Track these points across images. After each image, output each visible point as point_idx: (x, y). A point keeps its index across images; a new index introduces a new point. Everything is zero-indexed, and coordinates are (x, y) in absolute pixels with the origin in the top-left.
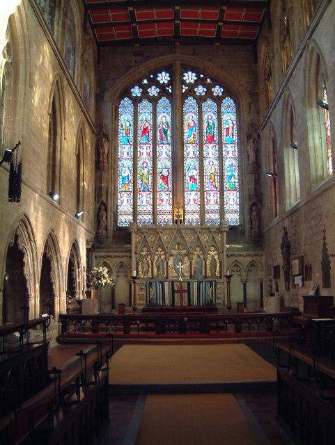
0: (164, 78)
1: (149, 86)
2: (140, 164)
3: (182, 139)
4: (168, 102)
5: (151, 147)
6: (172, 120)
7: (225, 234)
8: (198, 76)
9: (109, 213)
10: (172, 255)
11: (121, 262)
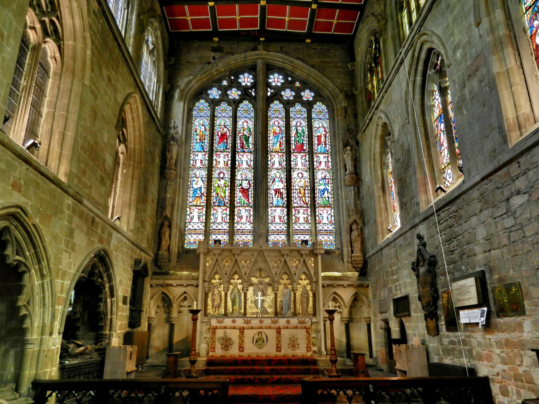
0: (246, 80)
1: (230, 87)
2: (215, 175)
3: (266, 147)
4: (250, 106)
5: (230, 155)
6: (255, 125)
7: (320, 257)
8: (285, 78)
9: (174, 230)
10: (251, 284)
11: (185, 293)
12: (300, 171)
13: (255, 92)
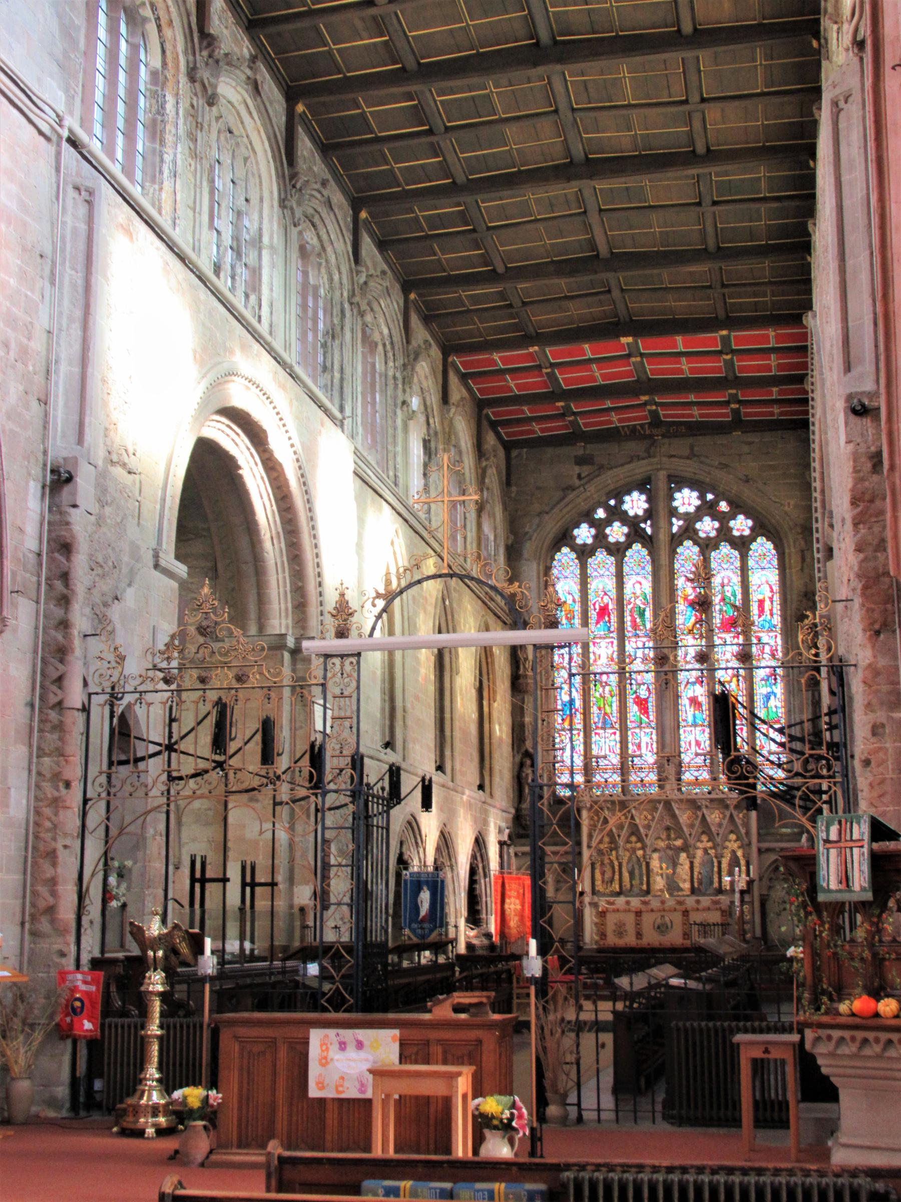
1: (608, 522)
8: (702, 497)
13: (652, 526)
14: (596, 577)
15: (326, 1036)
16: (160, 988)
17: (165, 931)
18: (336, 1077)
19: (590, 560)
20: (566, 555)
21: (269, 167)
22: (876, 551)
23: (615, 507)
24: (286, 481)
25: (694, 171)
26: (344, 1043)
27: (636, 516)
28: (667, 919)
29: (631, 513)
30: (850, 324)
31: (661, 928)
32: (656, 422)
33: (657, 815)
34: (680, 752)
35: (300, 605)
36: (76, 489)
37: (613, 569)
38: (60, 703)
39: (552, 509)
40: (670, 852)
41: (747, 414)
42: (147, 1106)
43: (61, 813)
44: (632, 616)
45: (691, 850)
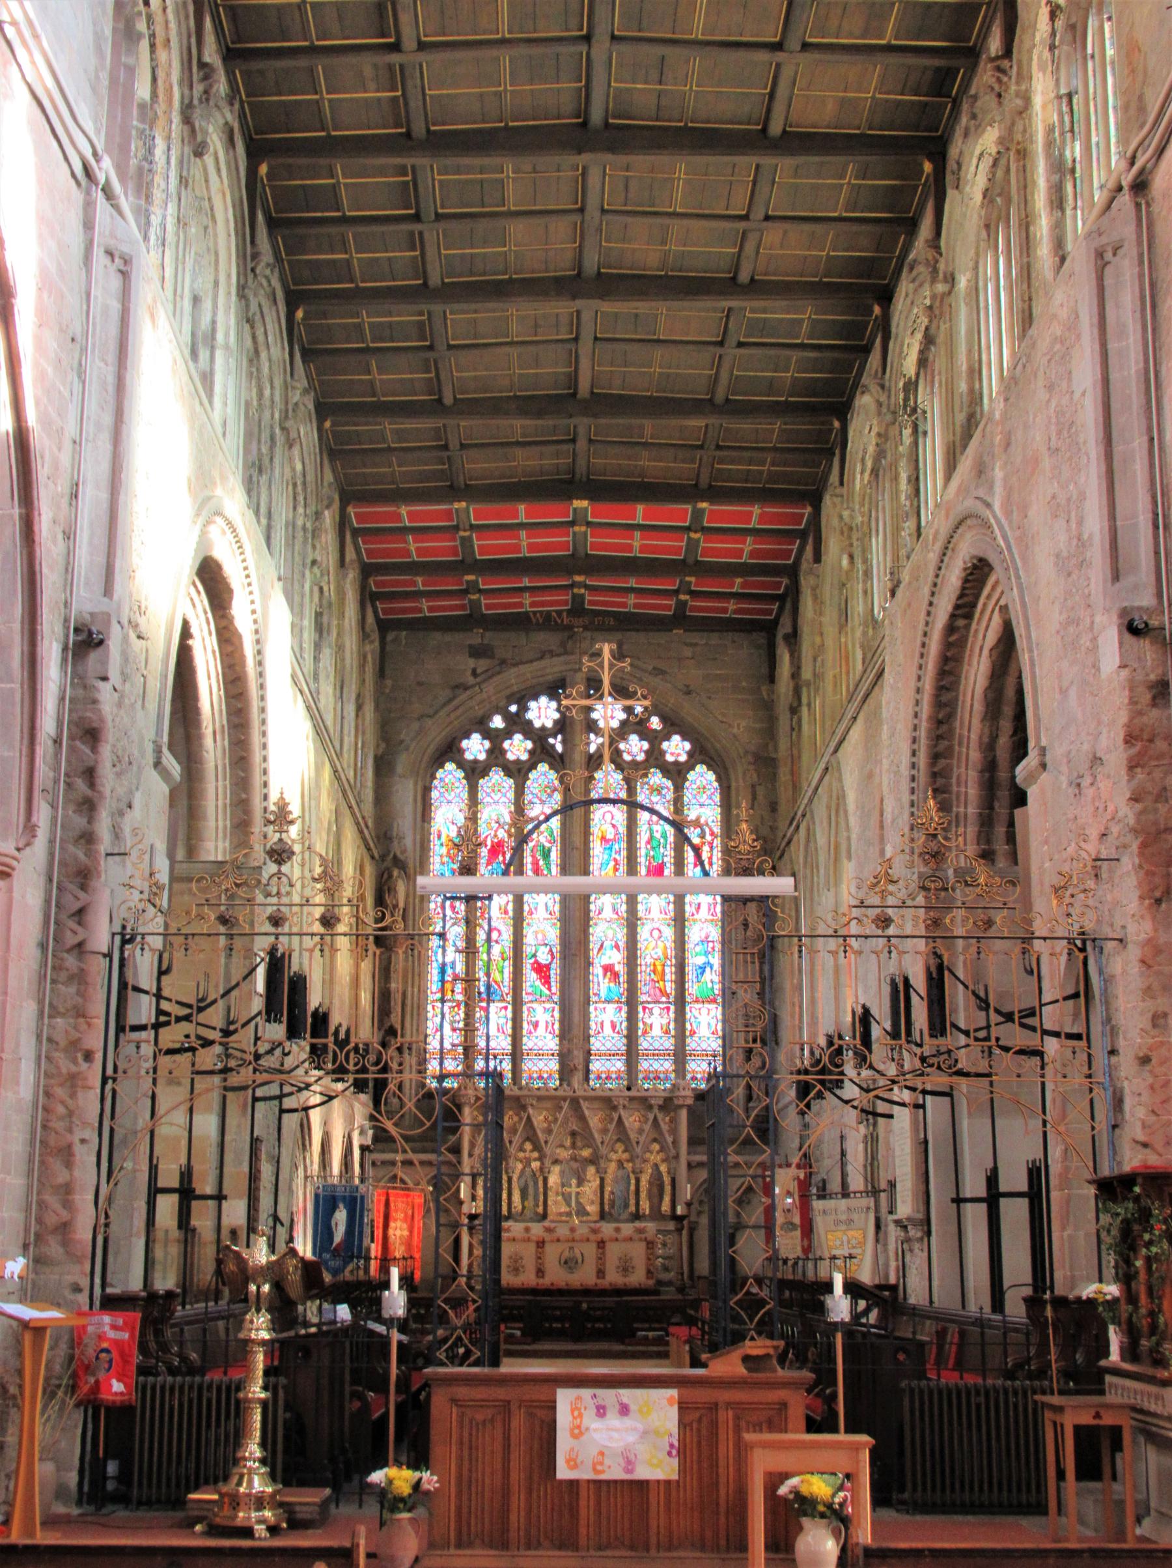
0: (543, 712)
1: (508, 734)
12: (656, 925)
13: (564, 742)
14: (488, 804)
15: (579, 1398)
16: (265, 1335)
17: (274, 1258)
18: (594, 1452)
19: (481, 781)
20: (450, 773)
21: (229, 241)
22: (1156, 801)
23: (517, 714)
24: (243, 657)
25: (726, 304)
26: (604, 1408)
27: (543, 728)
28: (577, 1251)
29: (537, 724)
30: (1118, 523)
31: (569, 1264)
32: (577, 609)
33: (560, 1117)
34: (589, 1036)
35: (241, 825)
36: (107, 656)
37: (511, 795)
38: (80, 945)
39: (436, 713)
40: (575, 1165)
41: (694, 608)
42: (249, 1495)
43: (80, 1094)
44: (533, 856)
45: (603, 1164)
